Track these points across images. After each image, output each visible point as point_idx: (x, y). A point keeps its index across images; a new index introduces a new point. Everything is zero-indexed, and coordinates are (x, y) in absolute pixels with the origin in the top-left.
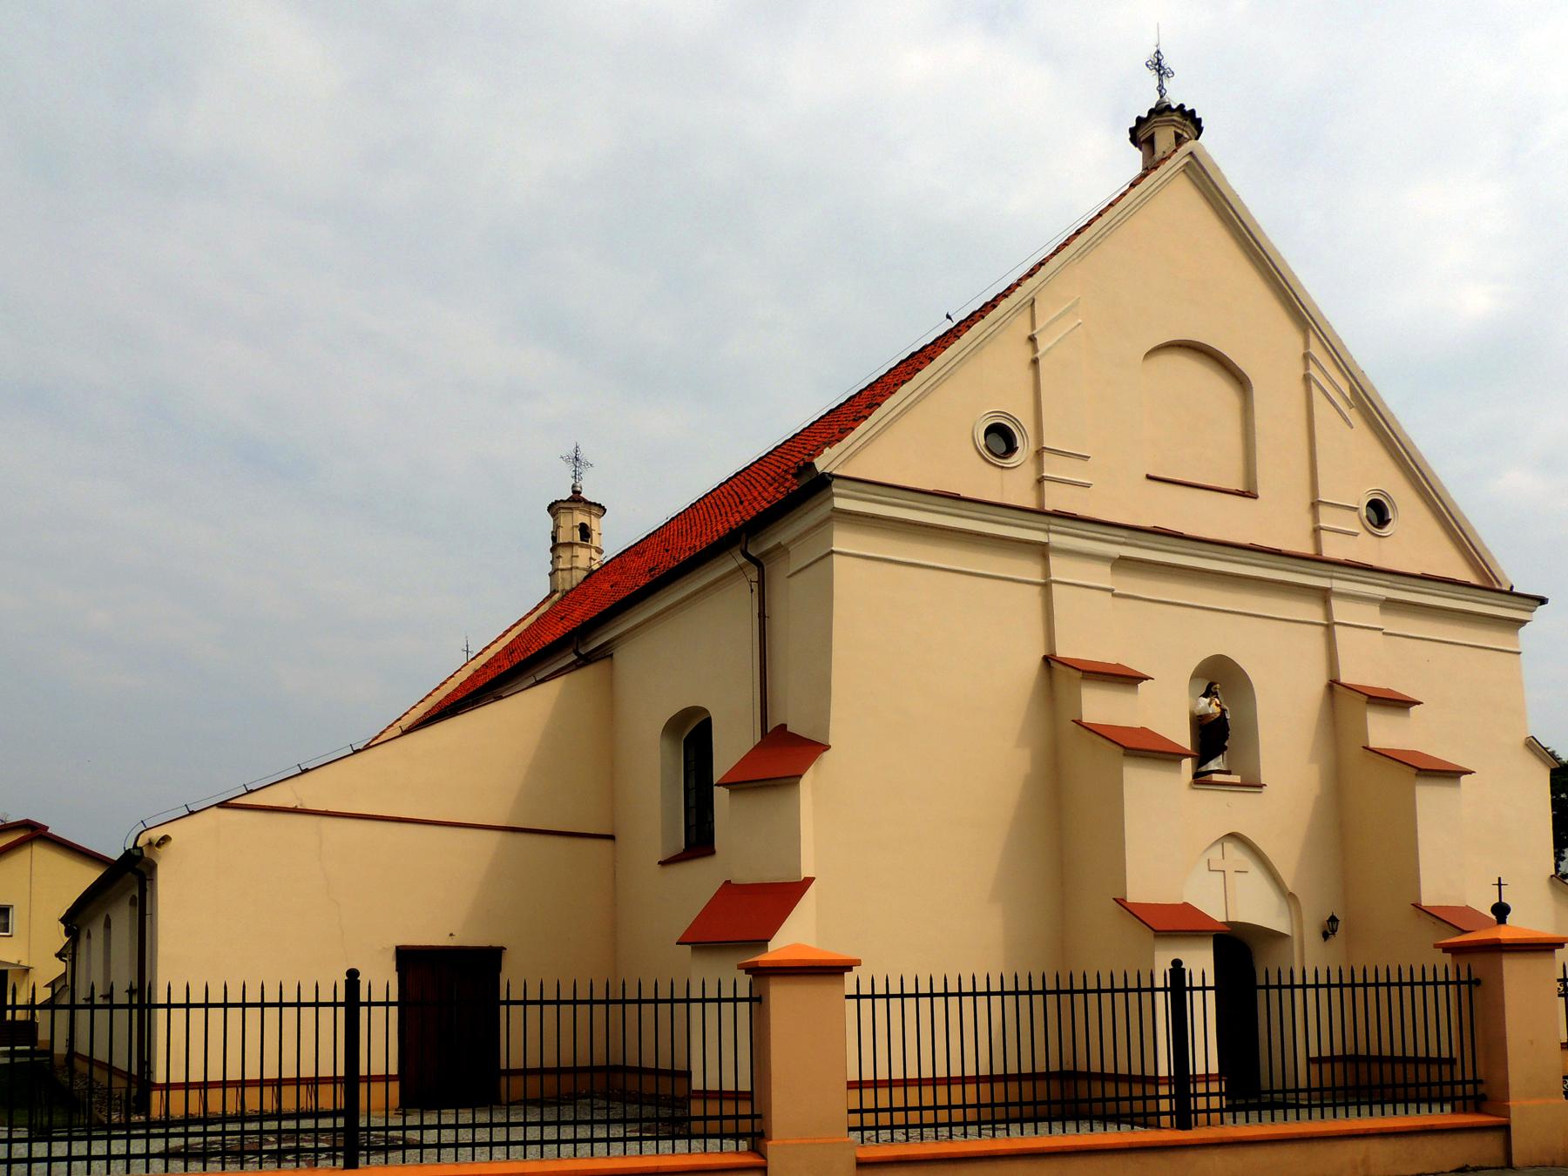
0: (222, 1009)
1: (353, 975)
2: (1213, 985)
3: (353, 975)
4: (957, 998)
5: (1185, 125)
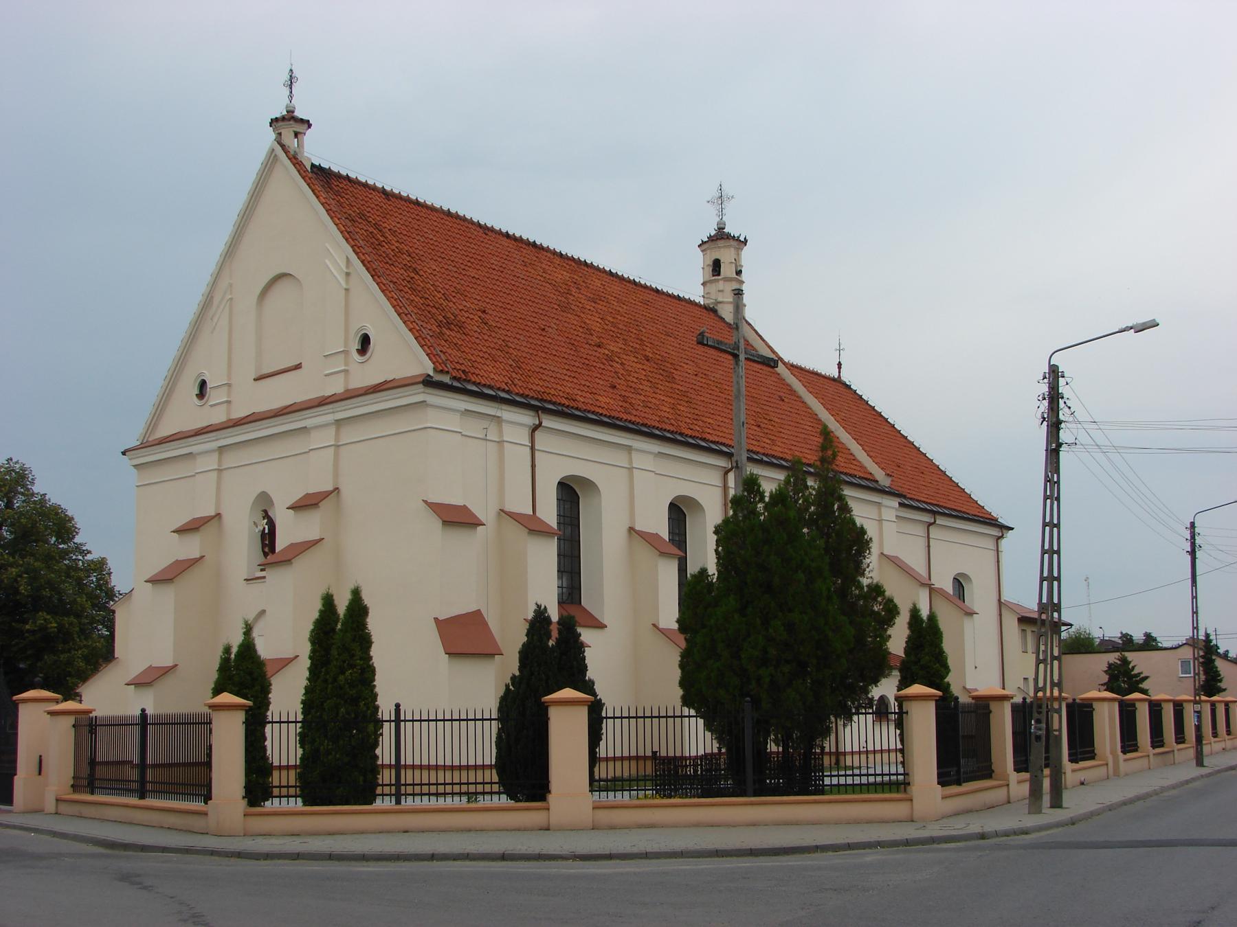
1: (398, 706)
3: (398, 706)
5: (291, 124)
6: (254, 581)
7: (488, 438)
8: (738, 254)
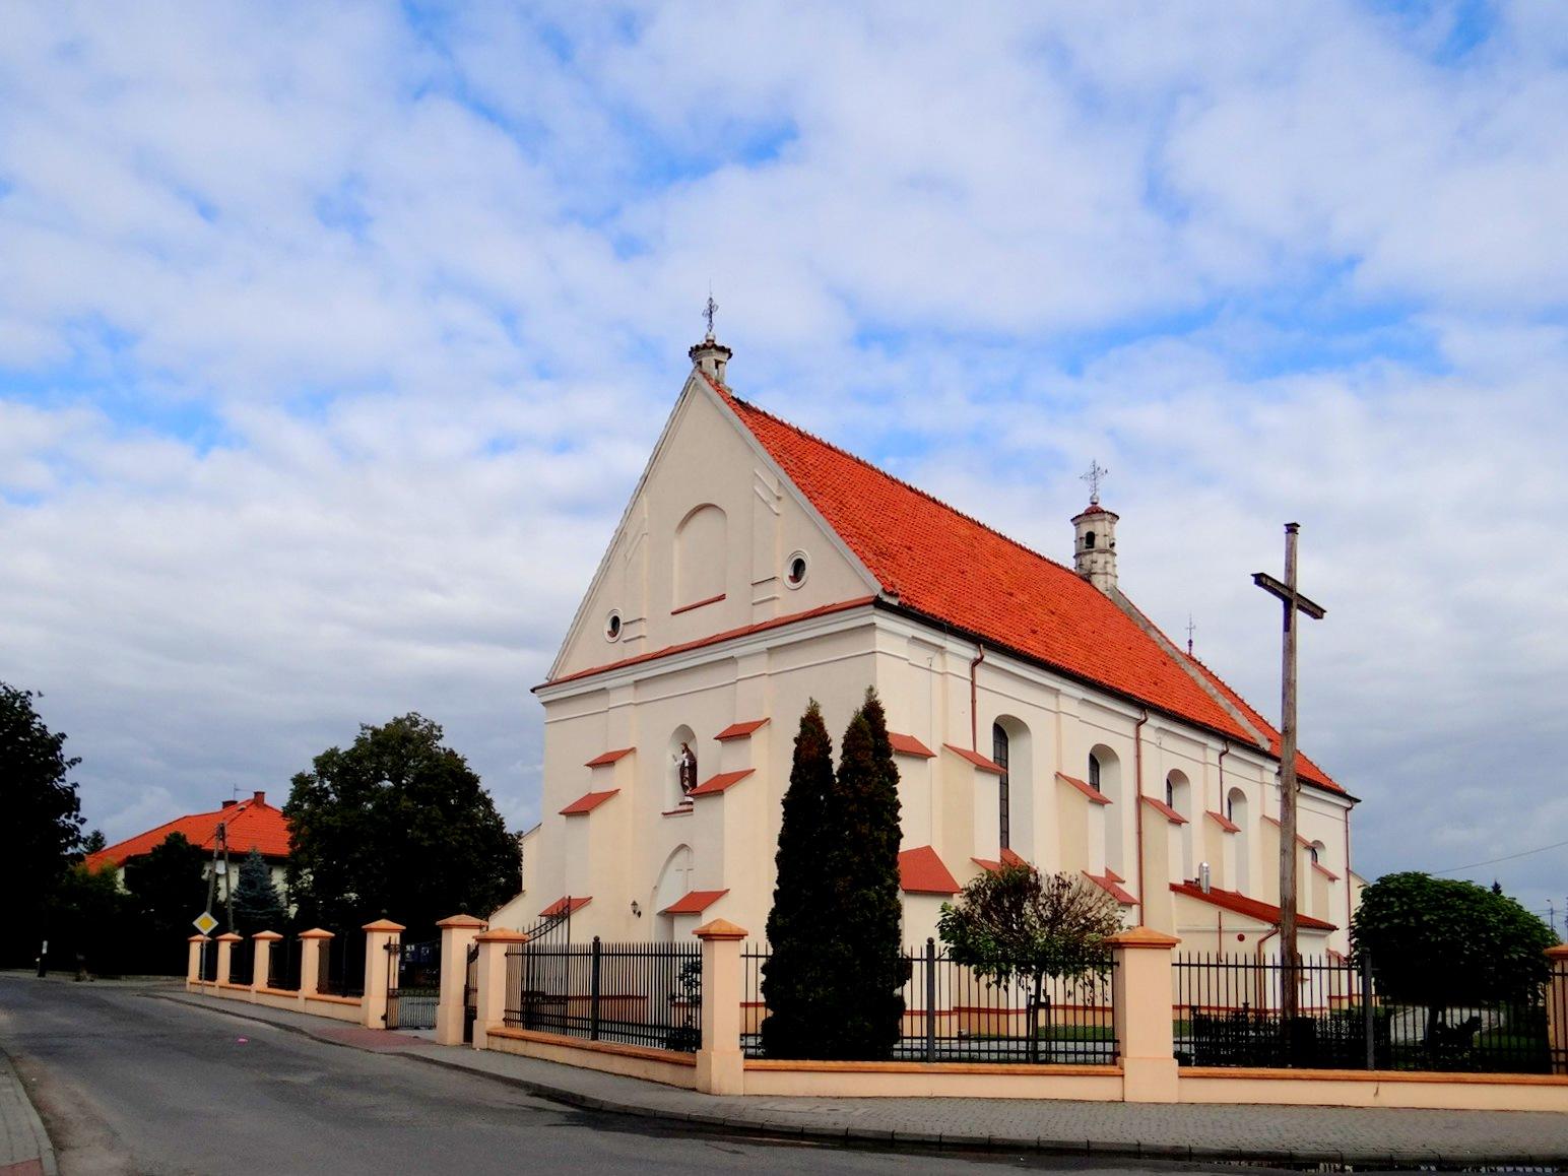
7: (933, 668)
8: (1111, 528)
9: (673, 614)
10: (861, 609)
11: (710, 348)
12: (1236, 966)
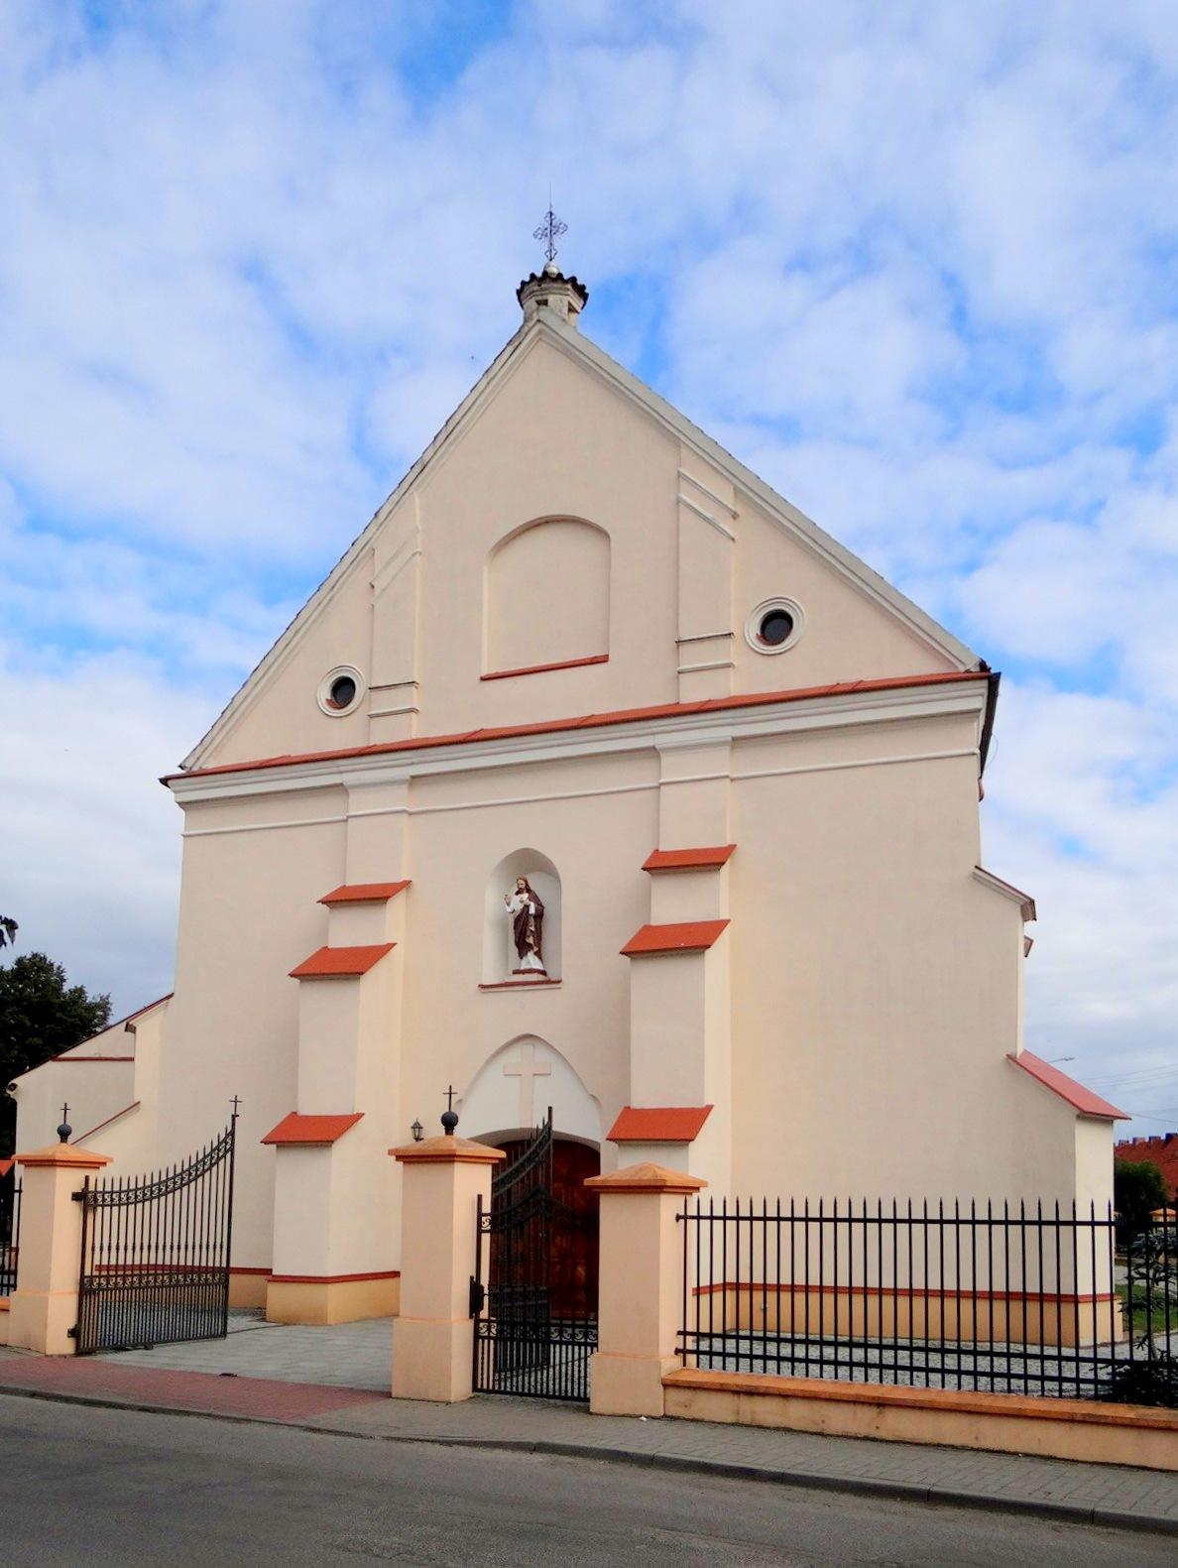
0: (847, 1224)
2: (489, 1211)
4: (749, 1222)
6: (504, 989)
9: (484, 679)
10: (949, 686)
11: (566, 282)
12: (765, 1219)
